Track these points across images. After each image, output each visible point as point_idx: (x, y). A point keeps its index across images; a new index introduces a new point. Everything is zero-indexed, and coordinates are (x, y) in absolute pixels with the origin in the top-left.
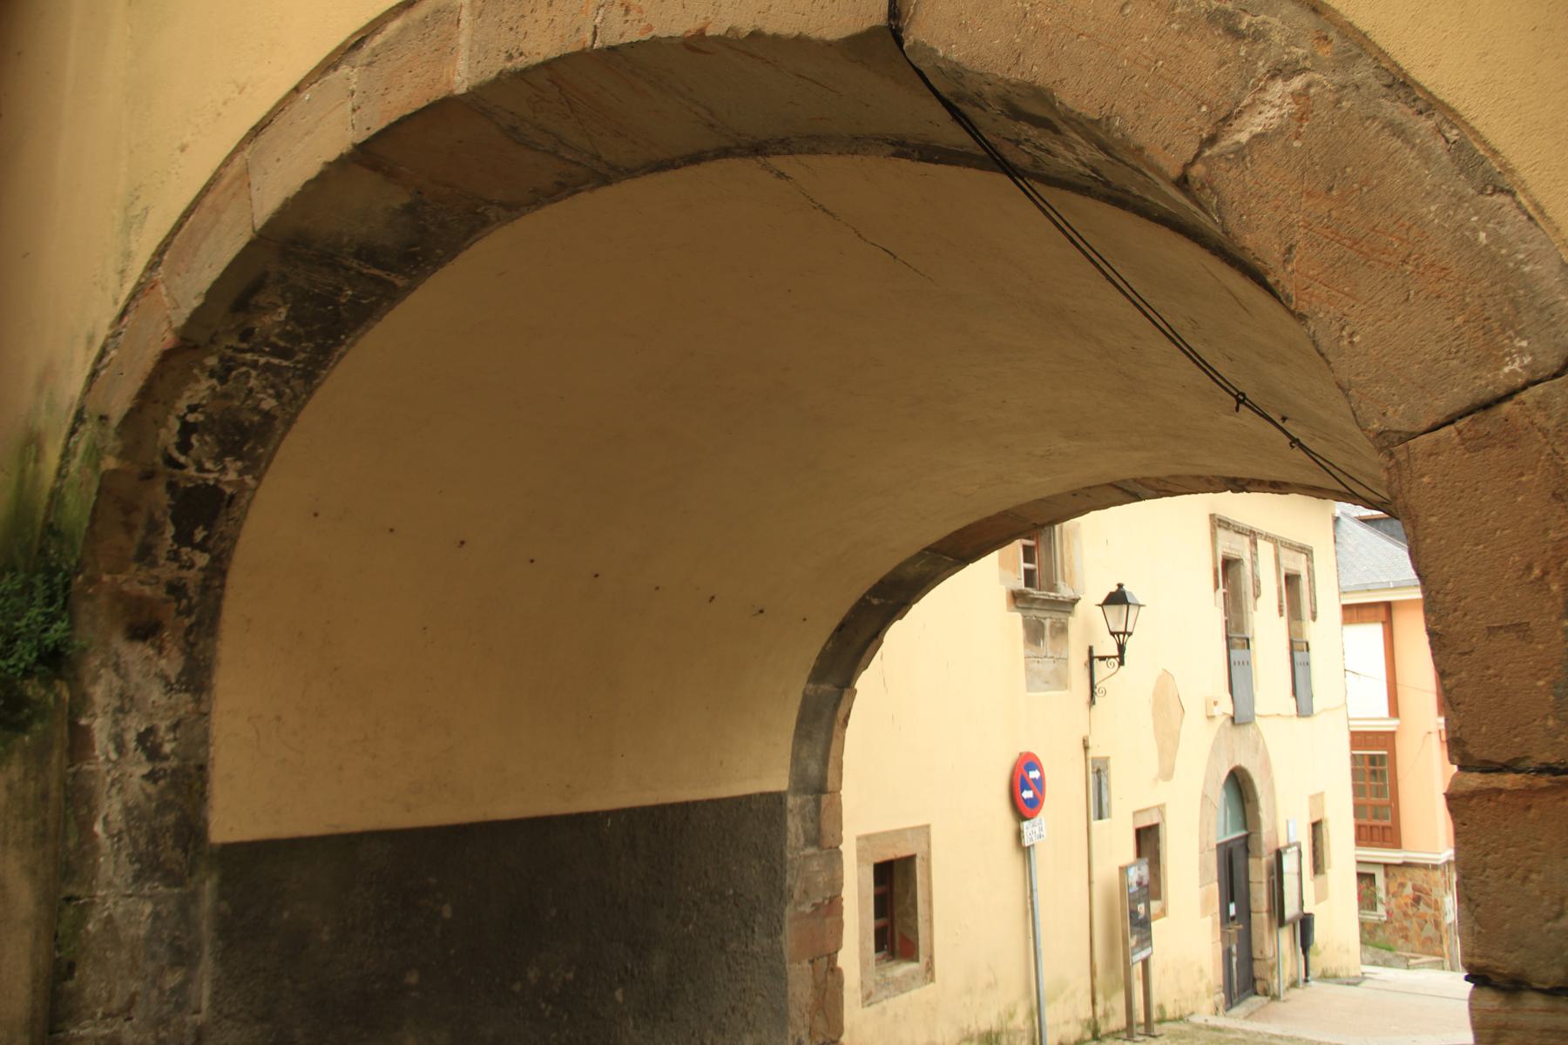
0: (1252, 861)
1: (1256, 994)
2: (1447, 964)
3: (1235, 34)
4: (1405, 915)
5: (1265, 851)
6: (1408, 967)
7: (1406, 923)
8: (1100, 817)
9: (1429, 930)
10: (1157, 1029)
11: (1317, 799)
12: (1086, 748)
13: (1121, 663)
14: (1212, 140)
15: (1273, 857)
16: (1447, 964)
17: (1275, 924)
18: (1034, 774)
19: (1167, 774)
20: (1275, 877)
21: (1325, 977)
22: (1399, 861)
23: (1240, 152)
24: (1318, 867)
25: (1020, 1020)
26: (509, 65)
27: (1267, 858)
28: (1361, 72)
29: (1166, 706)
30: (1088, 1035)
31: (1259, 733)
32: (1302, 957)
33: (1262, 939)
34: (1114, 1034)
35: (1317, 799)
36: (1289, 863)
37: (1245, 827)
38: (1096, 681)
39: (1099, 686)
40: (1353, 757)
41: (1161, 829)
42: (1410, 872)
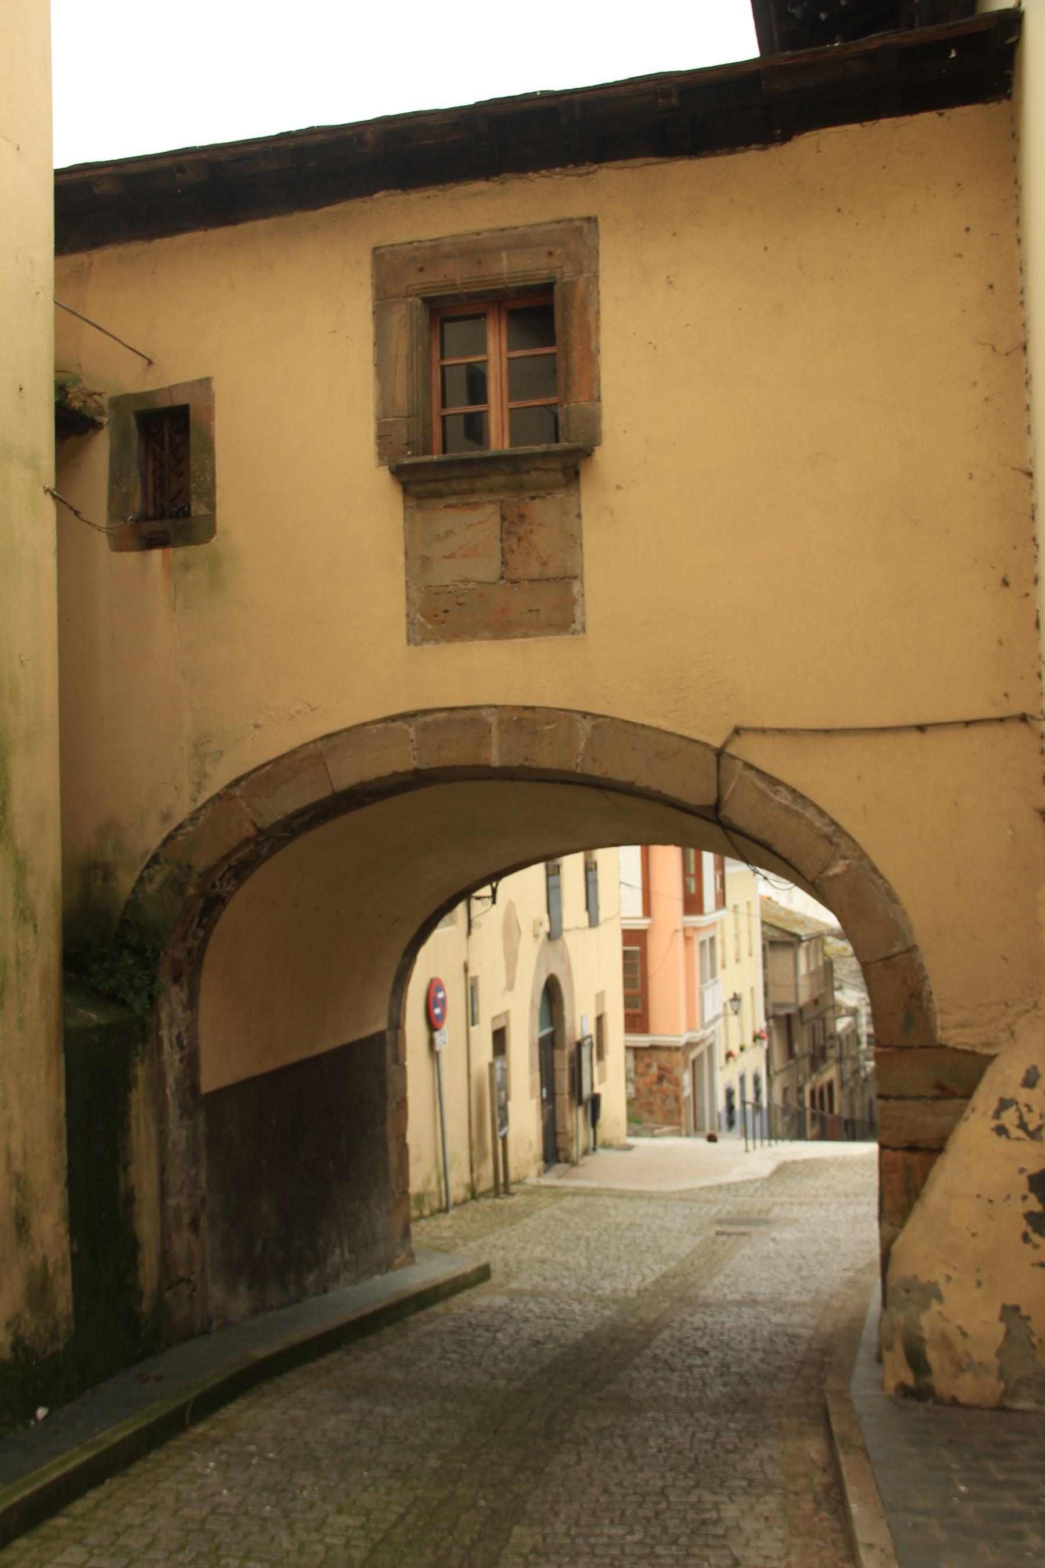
0: (557, 1053)
1: (559, 1161)
2: (684, 1132)
3: (831, 842)
4: (651, 1091)
5: (567, 1042)
6: (653, 1136)
7: (651, 1099)
8: (473, 1024)
9: (671, 1104)
10: (513, 1188)
11: (600, 997)
12: (466, 970)
13: (494, 902)
14: (821, 873)
15: (574, 1047)
16: (684, 1132)
17: (575, 1101)
18: (440, 995)
19: (510, 986)
20: (575, 1063)
21: (607, 1146)
22: (647, 1045)
23: (830, 878)
24: (601, 1056)
25: (433, 1186)
26: (526, 763)
27: (569, 1049)
28: (864, 863)
29: (510, 929)
30: (469, 1196)
31: (565, 945)
32: (591, 1131)
33: (564, 1116)
34: (485, 1194)
35: (600, 997)
36: (585, 1053)
37: (552, 1023)
38: (473, 915)
39: (475, 921)
40: (625, 953)
41: (507, 1031)
42: (656, 1054)
